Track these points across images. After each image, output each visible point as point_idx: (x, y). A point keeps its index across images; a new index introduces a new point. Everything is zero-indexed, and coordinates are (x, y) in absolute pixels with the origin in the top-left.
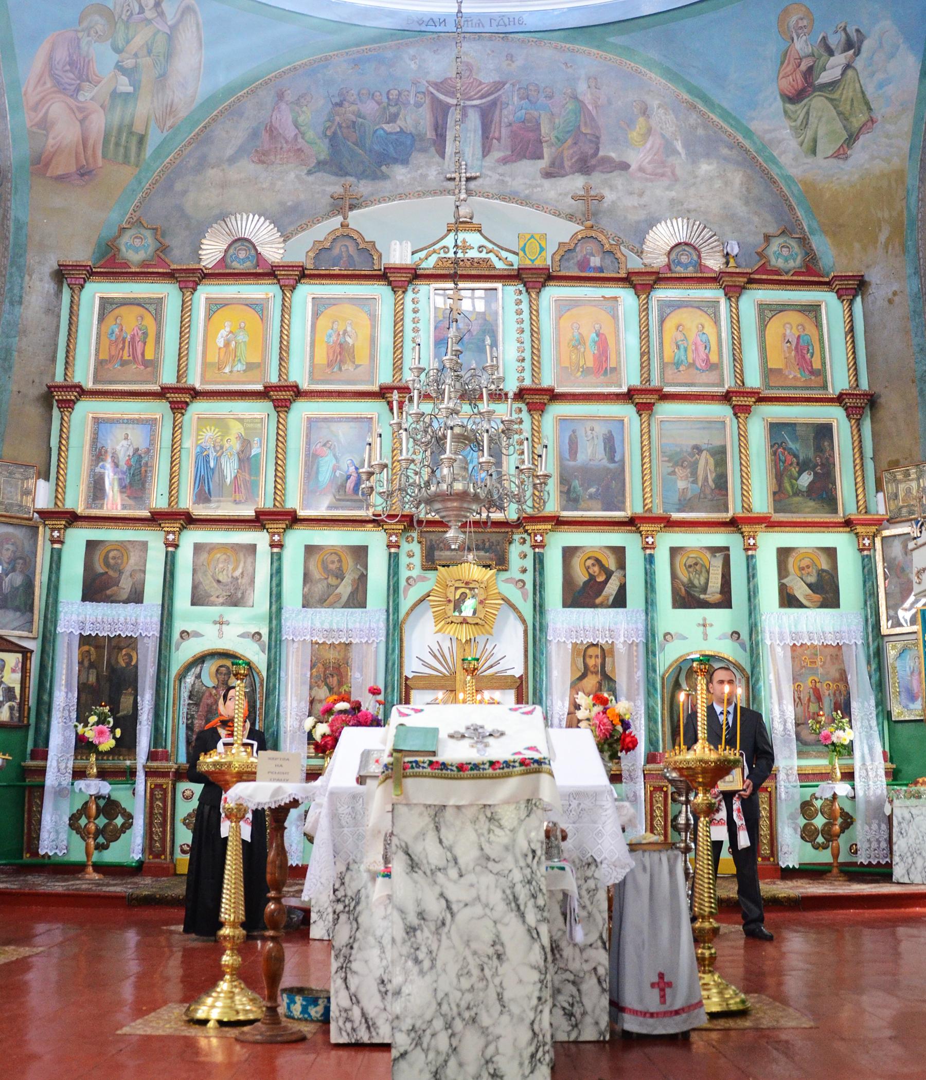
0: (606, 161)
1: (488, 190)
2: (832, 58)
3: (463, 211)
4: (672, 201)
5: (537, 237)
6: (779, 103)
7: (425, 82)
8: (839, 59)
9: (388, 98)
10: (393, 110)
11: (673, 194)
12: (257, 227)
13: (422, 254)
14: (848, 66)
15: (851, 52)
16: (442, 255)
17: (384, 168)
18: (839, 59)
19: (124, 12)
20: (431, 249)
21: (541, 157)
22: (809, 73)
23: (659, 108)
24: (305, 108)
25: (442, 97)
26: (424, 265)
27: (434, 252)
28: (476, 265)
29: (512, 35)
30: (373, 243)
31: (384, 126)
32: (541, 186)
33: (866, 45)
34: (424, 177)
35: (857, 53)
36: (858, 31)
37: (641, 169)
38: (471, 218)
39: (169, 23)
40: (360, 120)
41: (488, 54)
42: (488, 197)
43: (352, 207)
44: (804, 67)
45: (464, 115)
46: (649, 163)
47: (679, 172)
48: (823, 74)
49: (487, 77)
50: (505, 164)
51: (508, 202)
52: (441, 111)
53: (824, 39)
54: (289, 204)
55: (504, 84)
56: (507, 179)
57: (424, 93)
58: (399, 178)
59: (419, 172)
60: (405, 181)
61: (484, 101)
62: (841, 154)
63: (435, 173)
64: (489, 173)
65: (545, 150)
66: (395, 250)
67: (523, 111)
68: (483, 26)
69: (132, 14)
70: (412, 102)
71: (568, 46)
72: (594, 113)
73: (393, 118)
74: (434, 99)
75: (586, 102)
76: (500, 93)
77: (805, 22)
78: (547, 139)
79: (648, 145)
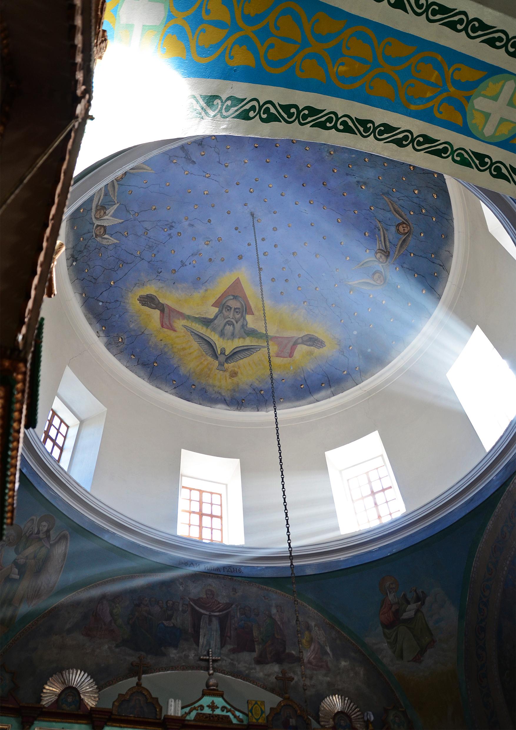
0: (290, 655)
1: (224, 668)
2: (409, 606)
3: (212, 682)
4: (329, 683)
5: (259, 703)
6: (380, 628)
7: (187, 598)
8: (413, 607)
9: (167, 605)
10: (170, 613)
11: (328, 679)
12: (82, 680)
13: (187, 710)
14: (418, 611)
15: (420, 603)
16: (199, 711)
17: (163, 648)
18: (413, 607)
19: (28, 532)
20: (193, 706)
21: (254, 651)
22: (397, 613)
23: (315, 626)
24: (117, 605)
25: (197, 608)
26: (188, 718)
27: (195, 708)
28: (220, 720)
29: (235, 578)
30: (157, 699)
31: (164, 622)
32: (255, 669)
33: (428, 599)
34: (187, 657)
35: (423, 603)
36: (422, 592)
37: (310, 662)
38: (217, 687)
39: (51, 542)
40: (150, 616)
41: (223, 587)
42: (224, 673)
43: (145, 672)
44: (393, 609)
45: (210, 621)
46: (314, 658)
47: (330, 665)
48: (404, 614)
49: (223, 599)
50: (234, 653)
51: (236, 678)
52: (197, 617)
53: (405, 595)
54: (103, 665)
55: (232, 605)
56: (236, 663)
57: (187, 605)
58: (172, 656)
59: (184, 653)
60: (176, 658)
61: (221, 613)
62: (417, 659)
63: (193, 655)
64: (225, 658)
65: (256, 646)
66: (171, 706)
67: (243, 622)
68: (220, 571)
69: (32, 533)
70: (181, 609)
71: (265, 587)
72: (281, 626)
73: (169, 618)
74: (193, 609)
75: (277, 620)
76: (229, 610)
77: (394, 586)
78: (257, 639)
79: (312, 648)
